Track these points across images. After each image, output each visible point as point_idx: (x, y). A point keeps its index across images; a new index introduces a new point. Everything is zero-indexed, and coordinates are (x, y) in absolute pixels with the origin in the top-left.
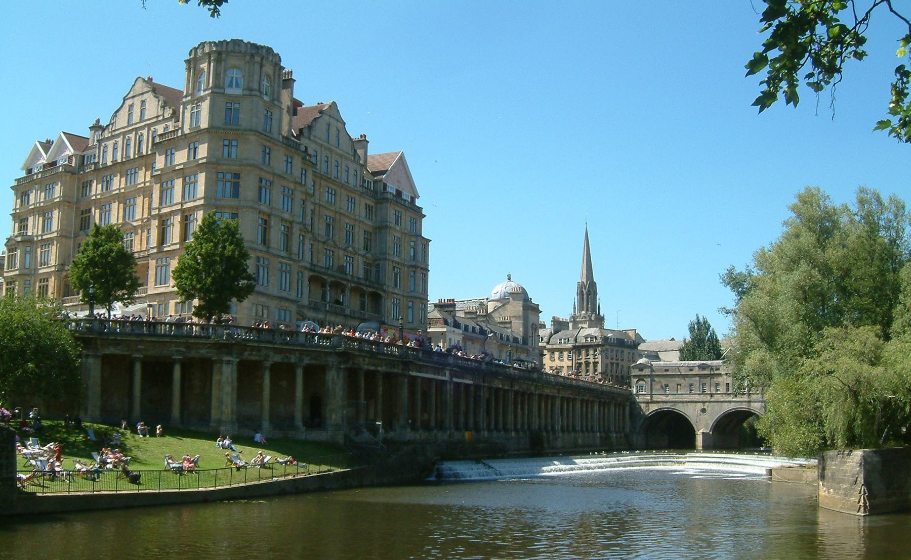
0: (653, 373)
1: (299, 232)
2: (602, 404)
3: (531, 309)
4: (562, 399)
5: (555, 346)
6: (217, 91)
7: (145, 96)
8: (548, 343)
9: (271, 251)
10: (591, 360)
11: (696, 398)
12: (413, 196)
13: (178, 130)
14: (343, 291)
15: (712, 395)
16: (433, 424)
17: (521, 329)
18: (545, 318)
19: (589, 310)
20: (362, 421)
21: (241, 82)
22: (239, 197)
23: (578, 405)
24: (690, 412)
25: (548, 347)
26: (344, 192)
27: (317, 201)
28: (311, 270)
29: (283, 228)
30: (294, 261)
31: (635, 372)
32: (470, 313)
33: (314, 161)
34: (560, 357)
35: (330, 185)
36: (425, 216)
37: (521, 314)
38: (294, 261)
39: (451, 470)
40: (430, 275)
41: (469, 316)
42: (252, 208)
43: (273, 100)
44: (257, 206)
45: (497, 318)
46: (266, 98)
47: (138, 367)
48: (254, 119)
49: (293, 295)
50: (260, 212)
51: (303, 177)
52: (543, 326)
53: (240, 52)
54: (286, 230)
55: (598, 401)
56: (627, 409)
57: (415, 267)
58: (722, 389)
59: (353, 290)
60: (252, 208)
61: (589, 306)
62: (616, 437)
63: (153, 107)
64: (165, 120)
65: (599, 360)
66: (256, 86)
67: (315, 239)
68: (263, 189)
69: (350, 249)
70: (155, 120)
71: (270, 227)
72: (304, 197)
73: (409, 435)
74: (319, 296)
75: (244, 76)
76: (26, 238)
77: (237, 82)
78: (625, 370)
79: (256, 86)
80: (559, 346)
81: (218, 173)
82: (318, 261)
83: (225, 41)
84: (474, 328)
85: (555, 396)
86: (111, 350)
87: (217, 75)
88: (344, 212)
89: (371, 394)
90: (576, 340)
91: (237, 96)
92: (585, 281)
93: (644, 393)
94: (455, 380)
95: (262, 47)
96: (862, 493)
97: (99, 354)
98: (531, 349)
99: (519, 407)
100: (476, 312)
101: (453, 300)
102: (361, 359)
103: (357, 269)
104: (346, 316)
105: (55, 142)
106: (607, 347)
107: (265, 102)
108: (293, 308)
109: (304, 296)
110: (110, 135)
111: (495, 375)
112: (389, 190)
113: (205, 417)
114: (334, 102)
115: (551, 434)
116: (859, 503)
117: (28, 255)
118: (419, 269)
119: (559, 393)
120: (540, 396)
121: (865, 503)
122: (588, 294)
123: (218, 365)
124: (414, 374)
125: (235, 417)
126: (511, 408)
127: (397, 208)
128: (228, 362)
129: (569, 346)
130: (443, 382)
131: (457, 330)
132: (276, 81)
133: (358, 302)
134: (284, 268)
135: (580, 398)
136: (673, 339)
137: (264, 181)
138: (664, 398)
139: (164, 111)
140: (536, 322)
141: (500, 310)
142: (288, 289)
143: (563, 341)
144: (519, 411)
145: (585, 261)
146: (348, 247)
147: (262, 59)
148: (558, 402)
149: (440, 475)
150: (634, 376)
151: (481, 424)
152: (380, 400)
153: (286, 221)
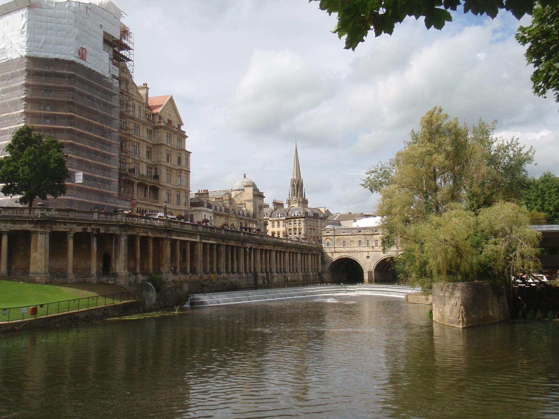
3: (258, 195)
4: (277, 251)
10: (297, 227)
11: (364, 249)
12: (179, 124)
17: (252, 208)
18: (268, 200)
19: (299, 196)
22: (177, 158)
25: (270, 219)
34: (278, 226)
37: (252, 199)
45: (237, 201)
52: (267, 206)
55: (300, 252)
56: (320, 257)
59: (139, 185)
78: (319, 232)
85: (272, 250)
94: (204, 241)
96: (461, 312)
98: (258, 221)
99: (248, 257)
100: (223, 198)
101: (207, 190)
102: (138, 229)
106: (307, 218)
111: (230, 239)
113: (26, 271)
115: (270, 274)
116: (459, 319)
118: (183, 172)
119: (274, 248)
120: (262, 250)
121: (463, 319)
122: (298, 186)
123: (35, 235)
125: (47, 270)
126: (259, 258)
128: (42, 233)
129: (284, 218)
135: (288, 251)
136: (350, 213)
138: (342, 249)
143: (280, 215)
145: (295, 166)
148: (274, 254)
150: (324, 236)
152: (151, 255)
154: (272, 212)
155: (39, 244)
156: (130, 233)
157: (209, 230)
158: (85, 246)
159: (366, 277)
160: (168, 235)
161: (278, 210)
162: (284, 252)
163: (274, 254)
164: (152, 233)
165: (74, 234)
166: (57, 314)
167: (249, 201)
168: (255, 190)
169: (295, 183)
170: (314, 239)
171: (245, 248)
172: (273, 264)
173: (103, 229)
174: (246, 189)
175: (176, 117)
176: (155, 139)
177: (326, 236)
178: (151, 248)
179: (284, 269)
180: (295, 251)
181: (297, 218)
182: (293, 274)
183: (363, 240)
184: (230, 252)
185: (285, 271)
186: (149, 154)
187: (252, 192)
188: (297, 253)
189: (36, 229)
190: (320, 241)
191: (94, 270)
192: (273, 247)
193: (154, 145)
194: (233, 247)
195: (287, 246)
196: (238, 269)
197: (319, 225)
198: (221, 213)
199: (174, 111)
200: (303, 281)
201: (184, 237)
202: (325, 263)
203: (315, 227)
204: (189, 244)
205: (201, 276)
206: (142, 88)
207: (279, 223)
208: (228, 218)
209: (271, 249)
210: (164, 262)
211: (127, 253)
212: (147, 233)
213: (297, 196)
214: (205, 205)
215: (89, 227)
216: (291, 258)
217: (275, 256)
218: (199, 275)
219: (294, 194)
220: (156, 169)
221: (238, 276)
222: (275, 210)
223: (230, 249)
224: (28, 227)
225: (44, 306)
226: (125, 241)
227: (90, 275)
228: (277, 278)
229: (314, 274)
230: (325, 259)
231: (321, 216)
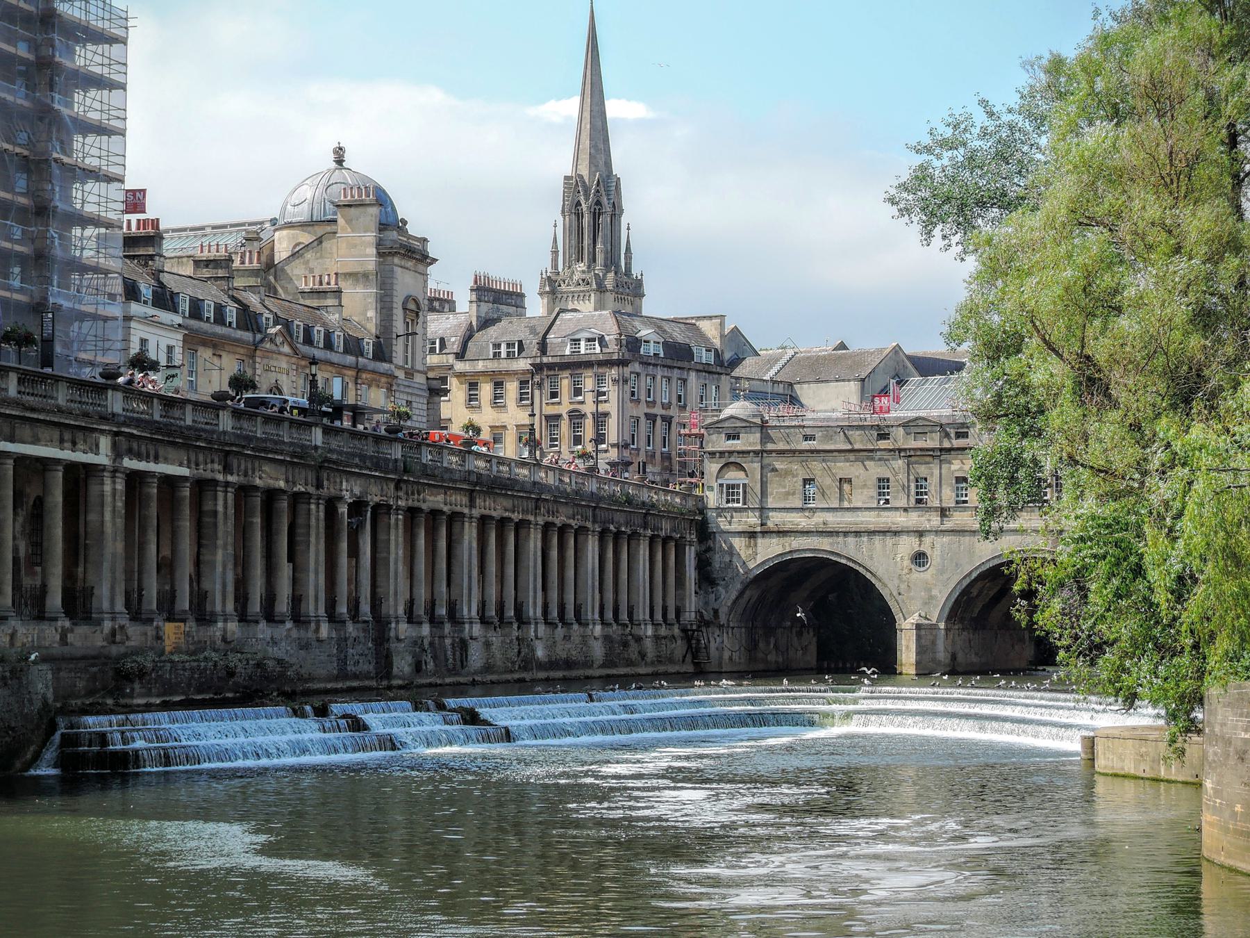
0: (770, 446)
4: (484, 521)
5: (480, 366)
8: (460, 356)
10: (589, 408)
15: (944, 512)
17: (371, 314)
23: (534, 542)
25: (460, 366)
31: (719, 443)
32: (208, 263)
41: (206, 273)
45: (301, 278)
52: (443, 304)
61: (599, 246)
62: (657, 638)
65: (611, 407)
80: (492, 366)
84: (219, 309)
85: (462, 515)
90: (543, 347)
92: (585, 172)
93: (740, 505)
94: (130, 463)
98: (400, 374)
102: (728, 515)
106: (637, 367)
115: (447, 628)
119: (472, 505)
120: (412, 512)
130: (91, 470)
135: (541, 520)
136: (842, 346)
141: (308, 255)
143: (503, 349)
148: (469, 534)
150: (712, 454)
151: (312, 607)
162: (521, 526)
163: (469, 534)
170: (664, 469)
172: (531, 586)
177: (722, 453)
179: (519, 608)
182: (560, 631)
184: (257, 520)
185: (521, 619)
188: (581, 531)
192: (465, 500)
200: (609, 663)
201: (36, 441)
203: (673, 412)
205: (113, 633)
207: (498, 385)
208: (253, 357)
209: (458, 509)
213: (593, 259)
216: (554, 554)
217: (475, 544)
218: (107, 625)
221: (295, 634)
229: (663, 631)
230: (717, 561)
231: (704, 357)
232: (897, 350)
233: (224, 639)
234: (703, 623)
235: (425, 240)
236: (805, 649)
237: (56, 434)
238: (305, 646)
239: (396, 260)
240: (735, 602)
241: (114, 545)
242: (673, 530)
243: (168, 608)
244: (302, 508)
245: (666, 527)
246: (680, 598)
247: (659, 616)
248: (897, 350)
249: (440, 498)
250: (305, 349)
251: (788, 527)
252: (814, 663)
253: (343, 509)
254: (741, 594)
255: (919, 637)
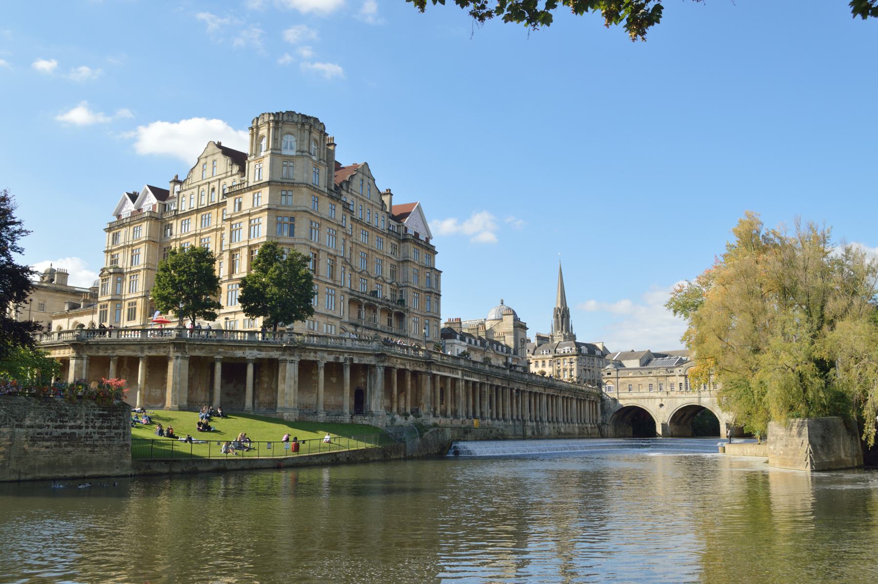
1: (341, 265)
2: (579, 401)
3: (520, 327)
4: (548, 395)
6: (276, 152)
7: (216, 157)
9: (320, 278)
13: (244, 183)
14: (375, 311)
16: (449, 412)
17: (512, 343)
18: (531, 335)
20: (395, 410)
21: (294, 144)
24: (651, 407)
26: (375, 234)
27: (354, 241)
28: (351, 294)
29: (329, 260)
30: (338, 286)
33: (352, 209)
35: (364, 228)
36: (437, 253)
38: (338, 286)
39: (465, 448)
40: (443, 300)
42: (305, 244)
43: (320, 160)
44: (308, 243)
46: (314, 158)
47: (218, 366)
48: (306, 175)
49: (337, 314)
50: (311, 248)
51: (344, 221)
53: (294, 121)
54: (331, 262)
56: (599, 405)
57: (430, 292)
58: (677, 388)
60: (305, 244)
62: (591, 428)
63: (223, 163)
64: (232, 175)
66: (306, 149)
67: (353, 270)
68: (313, 230)
69: (380, 278)
70: (224, 175)
71: (319, 260)
72: (344, 237)
73: (432, 420)
74: (356, 315)
75: (296, 141)
76: (117, 270)
77: (291, 144)
78: (596, 374)
79: (306, 149)
81: (277, 217)
82: (356, 287)
83: (281, 112)
86: (197, 353)
87: (275, 139)
88: (375, 249)
89: (402, 389)
91: (292, 156)
92: (559, 306)
94: (466, 378)
95: (310, 117)
96: (808, 452)
97: (187, 356)
98: (520, 358)
102: (395, 360)
103: (386, 292)
104: (377, 330)
105: (140, 195)
106: (581, 356)
107: (313, 161)
108: (338, 323)
109: (345, 314)
110: (187, 188)
112: (409, 232)
114: (366, 164)
115: (540, 423)
116: (806, 460)
117: (119, 284)
118: (433, 295)
119: (545, 391)
120: (530, 393)
121: (811, 460)
123: (284, 364)
124: (435, 372)
125: (296, 405)
127: (416, 247)
128: (292, 362)
131: (463, 343)
132: (322, 144)
133: (387, 320)
134: (330, 292)
135: (562, 395)
136: (633, 351)
137: (314, 224)
138: (627, 395)
139: (232, 168)
140: (524, 337)
142: (333, 309)
143: (545, 352)
144: (224, 565)
145: (560, 291)
146: (379, 277)
147: (310, 127)
148: (544, 398)
149: (457, 453)
152: (409, 392)
153: (331, 255)
154: (535, 349)
155: (287, 375)
156: (386, 364)
157: (471, 365)
158: (334, 380)
159: (659, 430)
160: (428, 369)
161: (544, 345)
162: (557, 396)
163: (544, 398)
164: (410, 366)
165: (325, 364)
166: (318, 453)
167: (508, 333)
168: (516, 319)
169: (559, 313)
171: (512, 389)
173: (357, 359)
174: (504, 317)
175: (424, 228)
176: (400, 255)
178: (409, 383)
180: (570, 396)
181: (568, 356)
182: (567, 424)
183: (655, 384)
184: (495, 393)
185: (558, 422)
186: (393, 273)
187: (512, 322)
188: (572, 398)
189: (284, 357)
190: (600, 384)
191: (347, 410)
192: (543, 390)
193: (398, 262)
194: (497, 387)
195: (561, 389)
196: (504, 415)
197: (596, 366)
198: (476, 347)
199: (421, 222)
200: (579, 434)
201: (444, 372)
202: (605, 413)
203: (591, 368)
204: (449, 381)
205: (463, 421)
206: (385, 194)
210: (423, 401)
211: (383, 388)
212: (404, 365)
213: (562, 329)
214: (458, 337)
215: (341, 357)
218: (461, 419)
219: (558, 327)
220: (401, 292)
221: (504, 423)
222: (539, 345)
223: (494, 388)
224: (275, 354)
225: (306, 442)
226: (382, 373)
227: (341, 414)
228: (548, 428)
229: (593, 426)
230: (606, 407)
232: (649, 351)
233: (488, 424)
234: (603, 423)
235: (525, 323)
236: (629, 432)
237: (449, 370)
238: (506, 427)
239: (519, 328)
240: (611, 418)
241: (462, 398)
242: (595, 399)
243: (475, 417)
244: (504, 391)
245: (592, 398)
246: (597, 417)
247: (591, 422)
248: (649, 351)
249: (537, 389)
250: (496, 352)
251: (625, 397)
252: (632, 435)
253: (514, 391)
254: (613, 416)
255: (662, 427)
